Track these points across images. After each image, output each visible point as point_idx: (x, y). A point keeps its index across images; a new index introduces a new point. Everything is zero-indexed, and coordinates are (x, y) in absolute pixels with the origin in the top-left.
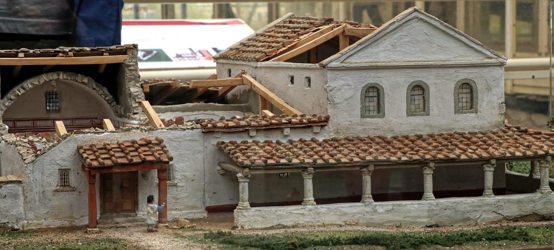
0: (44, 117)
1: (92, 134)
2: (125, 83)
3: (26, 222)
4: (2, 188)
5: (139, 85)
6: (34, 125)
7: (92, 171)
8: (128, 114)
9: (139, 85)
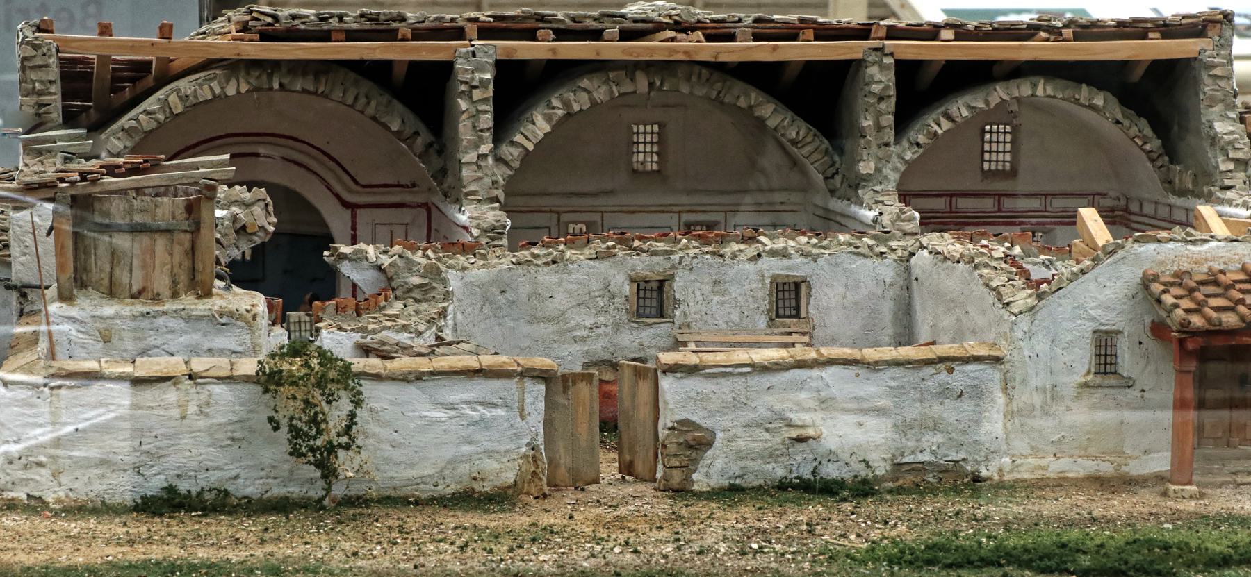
0: (974, 188)
1: (1180, 244)
2: (1199, 109)
3: (1007, 460)
4: (955, 373)
5: (1235, 116)
6: (951, 207)
7: (1189, 339)
8: (1205, 189)
9: (1235, 116)
